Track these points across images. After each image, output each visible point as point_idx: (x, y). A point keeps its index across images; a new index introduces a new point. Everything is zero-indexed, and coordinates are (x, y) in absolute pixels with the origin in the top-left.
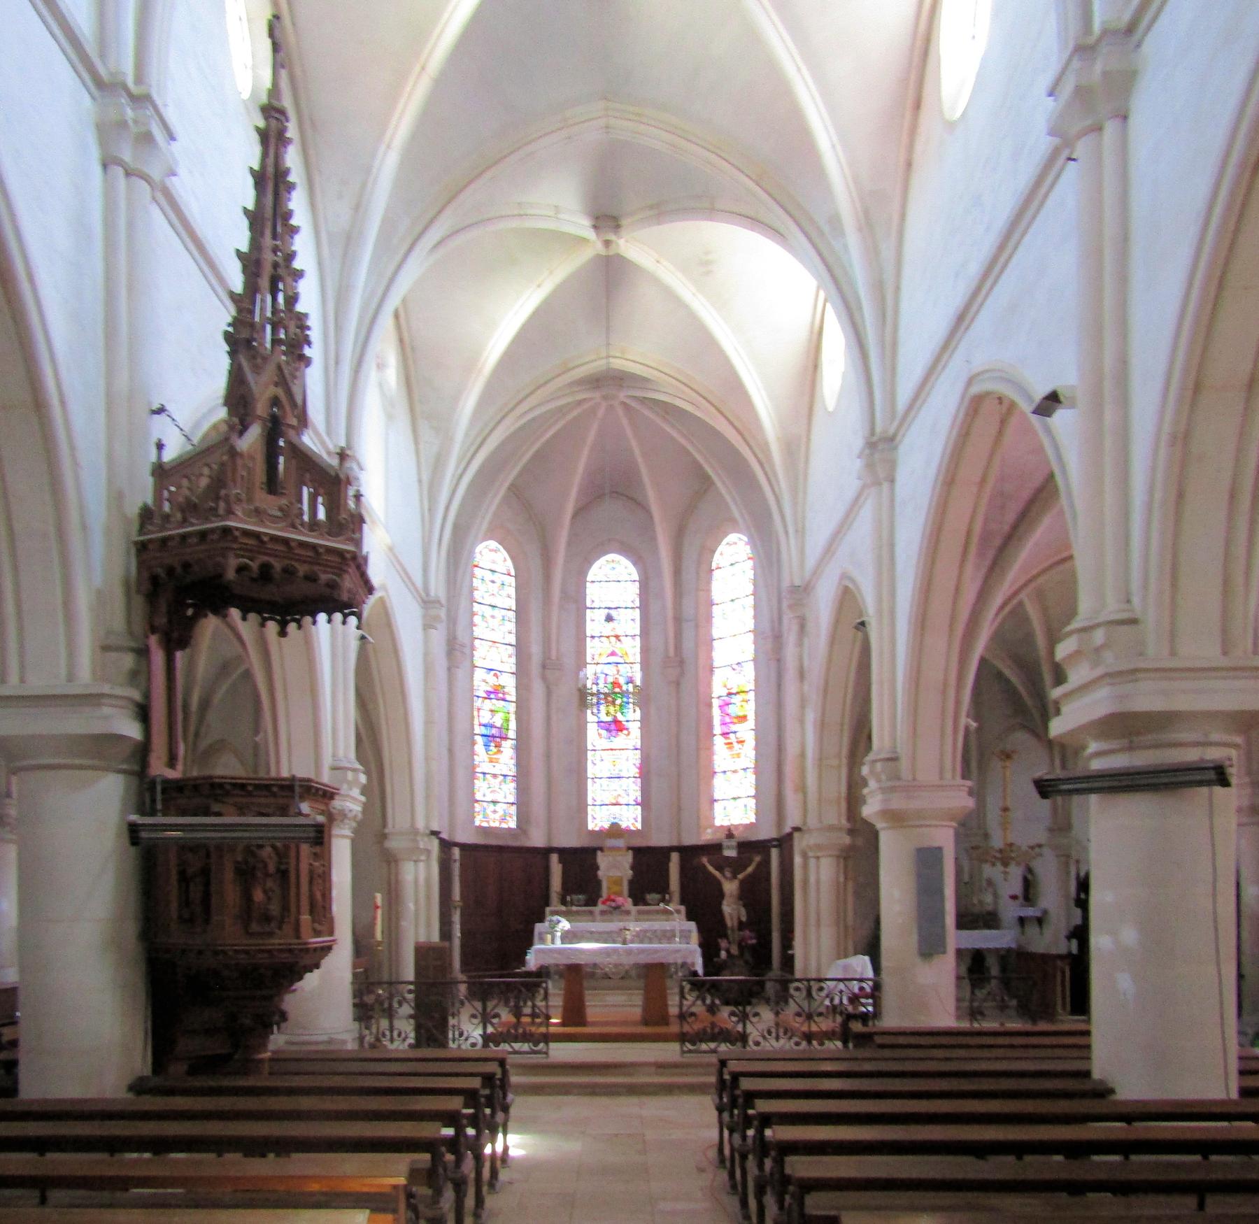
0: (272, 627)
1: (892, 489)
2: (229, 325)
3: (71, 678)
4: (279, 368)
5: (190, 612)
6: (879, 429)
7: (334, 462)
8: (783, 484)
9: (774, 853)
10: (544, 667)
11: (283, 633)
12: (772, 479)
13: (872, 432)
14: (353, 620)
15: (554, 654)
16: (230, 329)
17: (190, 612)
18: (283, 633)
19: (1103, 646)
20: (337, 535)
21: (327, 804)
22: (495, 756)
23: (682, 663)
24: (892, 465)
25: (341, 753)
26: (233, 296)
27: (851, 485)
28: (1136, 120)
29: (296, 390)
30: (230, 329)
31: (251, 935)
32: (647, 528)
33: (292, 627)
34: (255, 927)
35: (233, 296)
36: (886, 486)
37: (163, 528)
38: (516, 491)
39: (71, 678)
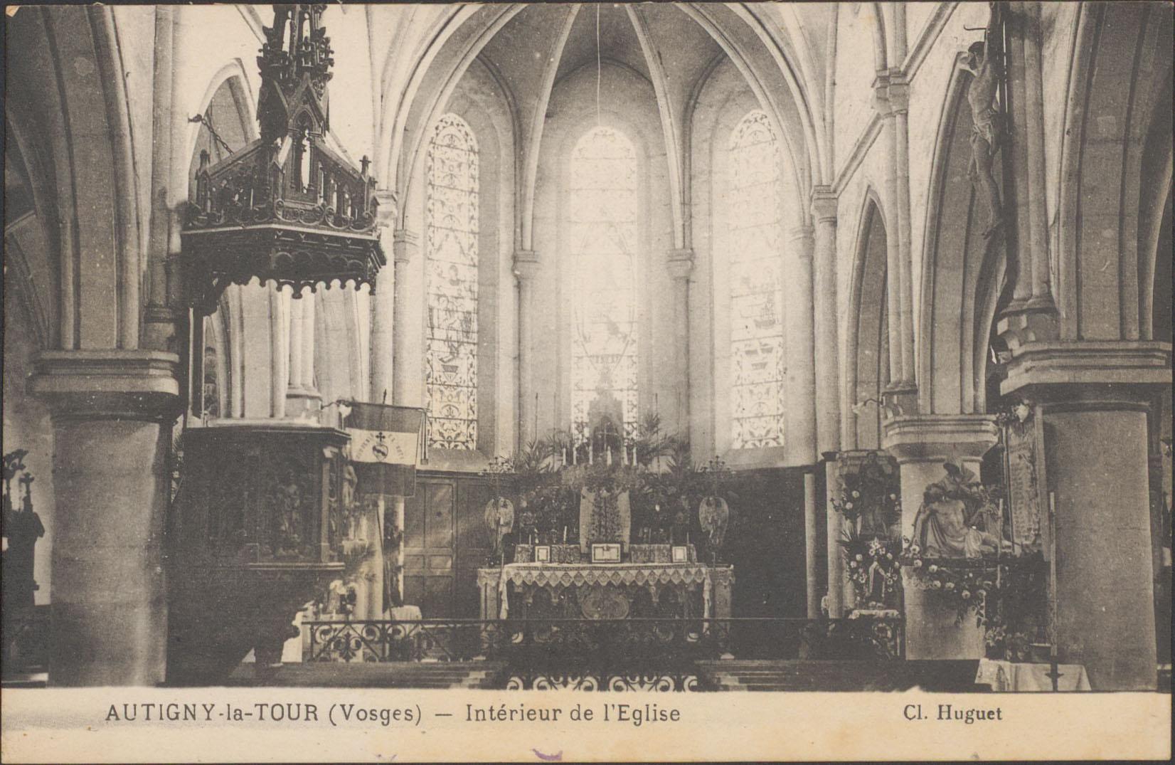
0: (287, 290)
1: (906, 122)
2: (260, 51)
3: (120, 346)
4: (308, 88)
5: (215, 282)
6: (891, 63)
7: (359, 167)
8: (806, 73)
9: (808, 478)
10: (515, 259)
11: (297, 295)
12: (796, 70)
13: (885, 67)
14: (365, 287)
15: (528, 245)
16: (261, 54)
17: (215, 282)
18: (297, 295)
19: (1027, 328)
20: (361, 227)
21: (340, 449)
22: (450, 364)
23: (691, 257)
24: (905, 98)
25: (298, 381)
26: (265, 30)
27: (868, 114)
28: (912, 112)
29: (322, 104)
30: (261, 54)
31: (278, 559)
32: (649, 98)
33: (306, 291)
34: (281, 552)
35: (265, 30)
36: (899, 119)
37: (209, 226)
38: (483, 57)
39: (120, 346)
